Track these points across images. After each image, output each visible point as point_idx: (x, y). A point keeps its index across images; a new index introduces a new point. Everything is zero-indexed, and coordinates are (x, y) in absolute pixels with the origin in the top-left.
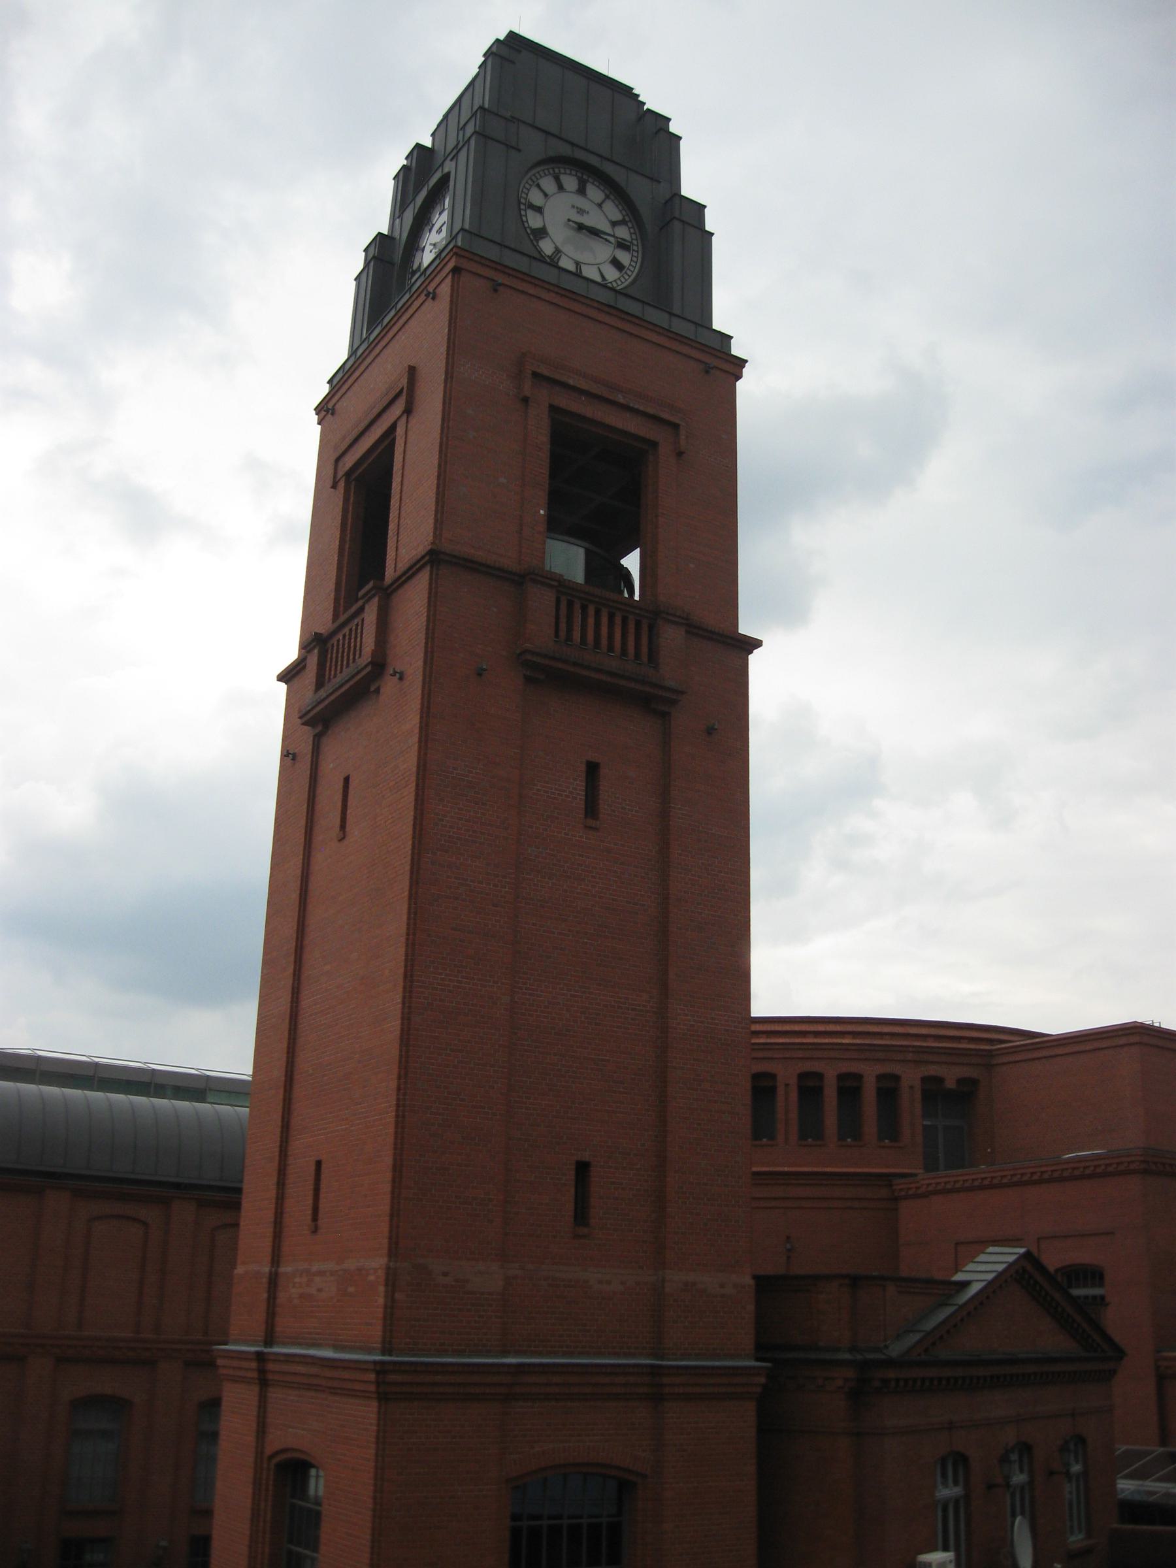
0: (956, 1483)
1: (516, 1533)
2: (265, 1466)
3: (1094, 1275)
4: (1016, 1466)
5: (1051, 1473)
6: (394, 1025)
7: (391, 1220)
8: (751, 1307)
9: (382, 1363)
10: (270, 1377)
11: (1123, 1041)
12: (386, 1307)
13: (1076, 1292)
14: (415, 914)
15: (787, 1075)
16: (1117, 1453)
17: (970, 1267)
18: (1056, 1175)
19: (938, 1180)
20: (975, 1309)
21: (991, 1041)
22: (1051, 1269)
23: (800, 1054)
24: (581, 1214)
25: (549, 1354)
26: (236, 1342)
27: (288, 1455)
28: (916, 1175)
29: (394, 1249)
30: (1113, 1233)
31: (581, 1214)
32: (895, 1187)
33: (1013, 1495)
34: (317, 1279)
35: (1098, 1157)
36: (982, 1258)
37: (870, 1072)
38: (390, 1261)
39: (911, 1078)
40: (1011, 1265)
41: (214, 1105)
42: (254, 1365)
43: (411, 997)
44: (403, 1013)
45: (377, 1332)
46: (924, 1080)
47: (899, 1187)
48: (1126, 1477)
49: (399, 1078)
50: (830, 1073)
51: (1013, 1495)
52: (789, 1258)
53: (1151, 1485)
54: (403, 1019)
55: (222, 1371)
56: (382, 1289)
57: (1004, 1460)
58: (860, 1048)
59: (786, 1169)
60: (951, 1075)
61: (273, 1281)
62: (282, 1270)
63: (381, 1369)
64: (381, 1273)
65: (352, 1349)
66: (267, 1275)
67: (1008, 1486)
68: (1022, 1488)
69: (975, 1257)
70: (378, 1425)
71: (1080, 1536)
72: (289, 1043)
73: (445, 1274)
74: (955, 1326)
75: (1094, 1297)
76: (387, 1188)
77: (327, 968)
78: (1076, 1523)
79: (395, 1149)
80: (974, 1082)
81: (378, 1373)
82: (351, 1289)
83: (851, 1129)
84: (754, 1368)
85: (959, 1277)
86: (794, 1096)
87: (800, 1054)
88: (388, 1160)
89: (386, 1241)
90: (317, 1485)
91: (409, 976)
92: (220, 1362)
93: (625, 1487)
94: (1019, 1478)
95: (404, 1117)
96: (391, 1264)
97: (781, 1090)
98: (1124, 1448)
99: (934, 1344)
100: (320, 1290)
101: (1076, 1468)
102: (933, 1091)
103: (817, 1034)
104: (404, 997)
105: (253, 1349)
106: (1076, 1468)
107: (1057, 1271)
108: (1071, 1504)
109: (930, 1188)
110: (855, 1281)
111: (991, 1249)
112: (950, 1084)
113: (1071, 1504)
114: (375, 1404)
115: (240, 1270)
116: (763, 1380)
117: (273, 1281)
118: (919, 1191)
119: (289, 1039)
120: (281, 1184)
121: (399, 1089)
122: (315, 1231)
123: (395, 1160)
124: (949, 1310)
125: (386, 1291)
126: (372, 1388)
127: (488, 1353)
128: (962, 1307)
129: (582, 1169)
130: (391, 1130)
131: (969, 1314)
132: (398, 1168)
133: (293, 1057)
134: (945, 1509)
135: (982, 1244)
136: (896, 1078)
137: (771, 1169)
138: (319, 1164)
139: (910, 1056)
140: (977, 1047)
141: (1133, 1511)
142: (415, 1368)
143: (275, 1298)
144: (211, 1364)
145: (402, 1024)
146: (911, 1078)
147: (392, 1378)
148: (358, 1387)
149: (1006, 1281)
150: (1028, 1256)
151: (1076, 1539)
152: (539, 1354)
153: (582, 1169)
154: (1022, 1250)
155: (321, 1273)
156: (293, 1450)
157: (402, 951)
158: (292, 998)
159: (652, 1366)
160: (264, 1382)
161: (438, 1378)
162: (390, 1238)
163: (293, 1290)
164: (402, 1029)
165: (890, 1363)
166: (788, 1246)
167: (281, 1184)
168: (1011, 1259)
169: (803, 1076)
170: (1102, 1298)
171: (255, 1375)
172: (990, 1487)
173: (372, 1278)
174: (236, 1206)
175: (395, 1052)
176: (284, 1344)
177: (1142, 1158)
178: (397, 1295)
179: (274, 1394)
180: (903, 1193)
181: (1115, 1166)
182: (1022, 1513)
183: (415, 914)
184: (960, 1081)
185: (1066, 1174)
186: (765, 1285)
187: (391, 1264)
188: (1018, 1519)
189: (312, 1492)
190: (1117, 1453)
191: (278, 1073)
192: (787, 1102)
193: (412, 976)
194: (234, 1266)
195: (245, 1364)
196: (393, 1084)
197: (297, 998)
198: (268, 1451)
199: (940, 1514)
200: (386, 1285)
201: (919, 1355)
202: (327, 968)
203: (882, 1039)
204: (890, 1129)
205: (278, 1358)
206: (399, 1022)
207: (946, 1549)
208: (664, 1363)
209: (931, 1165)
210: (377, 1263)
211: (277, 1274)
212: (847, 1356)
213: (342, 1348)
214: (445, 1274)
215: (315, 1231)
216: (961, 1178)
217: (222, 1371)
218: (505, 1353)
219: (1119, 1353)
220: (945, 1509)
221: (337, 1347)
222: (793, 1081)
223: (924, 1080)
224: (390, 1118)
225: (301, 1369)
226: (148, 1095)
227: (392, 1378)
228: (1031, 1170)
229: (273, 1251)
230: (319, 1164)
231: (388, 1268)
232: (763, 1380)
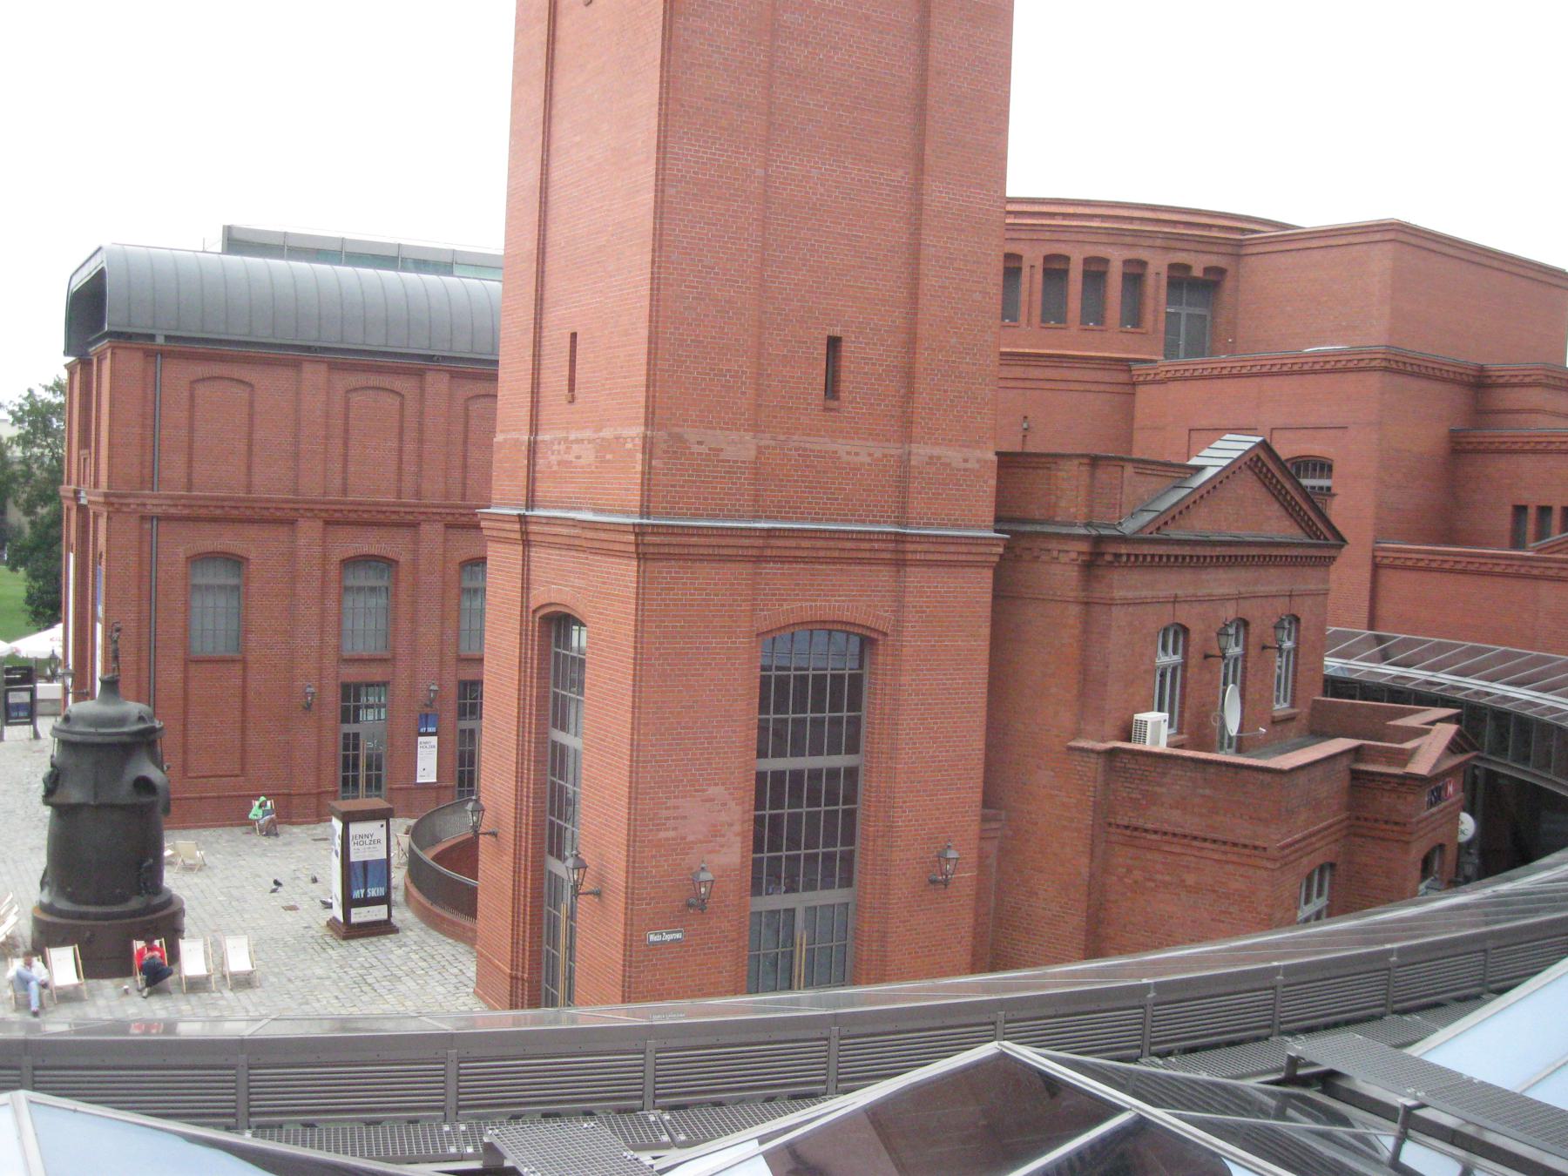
0: (1175, 653)
1: (765, 682)
2: (530, 619)
3: (1323, 467)
4: (1232, 641)
5: (1264, 648)
6: (648, 197)
7: (647, 391)
8: (993, 482)
9: (640, 525)
10: (532, 537)
11: (1378, 237)
12: (643, 473)
13: (1306, 482)
14: (668, 82)
15: (1033, 256)
16: (1327, 633)
17: (1206, 452)
18: (1296, 368)
19: (1177, 368)
20: (1208, 492)
21: (1243, 231)
22: (1283, 458)
23: (1047, 236)
24: (832, 387)
25: (798, 520)
26: (498, 505)
27: (553, 609)
28: (1155, 361)
29: (650, 419)
30: (1346, 428)
31: (832, 387)
32: (1133, 372)
33: (1227, 666)
34: (575, 446)
35: (1341, 353)
36: (1218, 444)
37: (1117, 257)
38: (647, 429)
39: (1158, 264)
40: (1247, 452)
41: (463, 279)
42: (517, 527)
43: (664, 169)
44: (656, 185)
45: (635, 498)
46: (1172, 267)
47: (1138, 372)
48: (1331, 656)
49: (654, 250)
50: (1077, 256)
51: (1227, 666)
52: (1025, 436)
53: (1354, 663)
54: (656, 191)
55: (485, 532)
56: (639, 456)
57: (1223, 633)
58: (1109, 232)
59: (1027, 351)
60: (1198, 264)
61: (533, 450)
62: (540, 438)
63: (639, 531)
64: (639, 442)
65: (611, 512)
66: (527, 443)
67: (1224, 657)
68: (1236, 660)
69: (1212, 443)
70: (638, 582)
71: (1285, 705)
72: (540, 216)
73: (700, 443)
74: (1188, 507)
75: (1321, 488)
76: (643, 358)
77: (578, 139)
78: (1282, 695)
79: (650, 321)
80: (1221, 272)
81: (637, 535)
82: (609, 457)
83: (1094, 314)
84: (993, 538)
85: (1194, 461)
86: (1039, 276)
87: (1047, 236)
88: (645, 333)
89: (643, 410)
90: (579, 638)
91: (662, 147)
92: (483, 524)
93: (867, 643)
94: (1234, 650)
95: (658, 289)
96: (649, 433)
97: (1026, 271)
98: (1334, 628)
99: (1166, 523)
100: (578, 457)
101: (1288, 644)
102: (1179, 279)
103: (1065, 216)
104: (657, 169)
105: (515, 512)
106: (1288, 644)
107: (1287, 460)
108: (1279, 677)
109: (1169, 375)
110: (1094, 461)
111: (1228, 436)
112: (1197, 272)
113: (1279, 677)
114: (628, 570)
115: (499, 438)
116: (1000, 550)
117: (533, 450)
118: (1158, 378)
119: (540, 211)
120: (537, 356)
121: (653, 262)
122: (572, 401)
123: (650, 332)
124: (1184, 492)
125: (643, 460)
126: (632, 548)
127: (741, 518)
128: (1195, 490)
129: (834, 344)
130: (647, 303)
131: (1202, 497)
132: (653, 340)
133: (545, 230)
134: (1163, 675)
135: (1219, 431)
136: (1143, 264)
137: (1014, 350)
138: (574, 336)
139: (1158, 242)
140: (1228, 236)
141: (1337, 686)
142: (670, 530)
143: (534, 465)
144: (477, 527)
145: (656, 196)
146: (1158, 264)
147: (648, 539)
148: (617, 547)
149: (1240, 468)
150: (1264, 445)
151: (1281, 708)
152: (789, 519)
153: (834, 344)
154: (1258, 439)
155: (579, 441)
156: (551, 604)
157: (654, 122)
158: (542, 170)
159: (897, 534)
160: (526, 543)
161: (694, 540)
162: (647, 407)
163: (553, 457)
164: (656, 202)
165: (1123, 539)
166: (1025, 426)
167: (537, 356)
168: (1247, 446)
169: (1048, 259)
170: (1329, 489)
171: (518, 536)
172: (1206, 657)
173: (629, 446)
174: (493, 377)
175: (648, 224)
176: (545, 507)
177: (1384, 356)
178: (654, 462)
179: (536, 553)
180: (1141, 379)
181: (1367, 361)
182: (1234, 682)
183: (668, 82)
184: (1207, 270)
185: (1306, 367)
186: (1008, 462)
187: (649, 433)
188: (1231, 686)
189: (575, 644)
190: (1327, 633)
191: (531, 245)
192: (1032, 282)
193: (665, 148)
194: (493, 432)
195: (508, 526)
196: (648, 258)
197: (547, 170)
198: (533, 606)
199: (1158, 678)
200: (644, 452)
201: (1151, 533)
202: (578, 139)
203: (1131, 223)
204: (1134, 316)
205: (539, 520)
206: (652, 195)
207: (1160, 709)
208: (908, 531)
209: (1170, 351)
210: (635, 432)
211: (535, 442)
212: (1082, 531)
213: (602, 511)
214: (700, 443)
215: (572, 401)
216: (1200, 366)
217: (485, 532)
218: (756, 518)
219: (1342, 541)
220: (1163, 675)
221: (596, 511)
222: (1039, 264)
223: (1172, 267)
224: (645, 290)
225: (565, 531)
226: (395, 268)
227: (648, 539)
228: (1272, 362)
229: (531, 420)
230: (574, 336)
231: (645, 437)
232: (1000, 550)
